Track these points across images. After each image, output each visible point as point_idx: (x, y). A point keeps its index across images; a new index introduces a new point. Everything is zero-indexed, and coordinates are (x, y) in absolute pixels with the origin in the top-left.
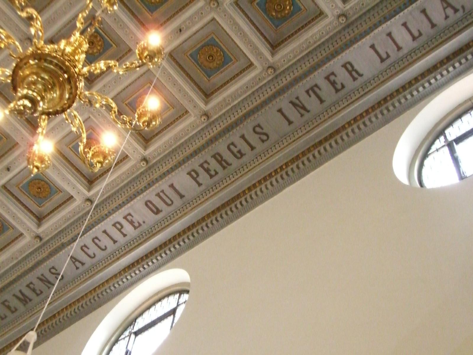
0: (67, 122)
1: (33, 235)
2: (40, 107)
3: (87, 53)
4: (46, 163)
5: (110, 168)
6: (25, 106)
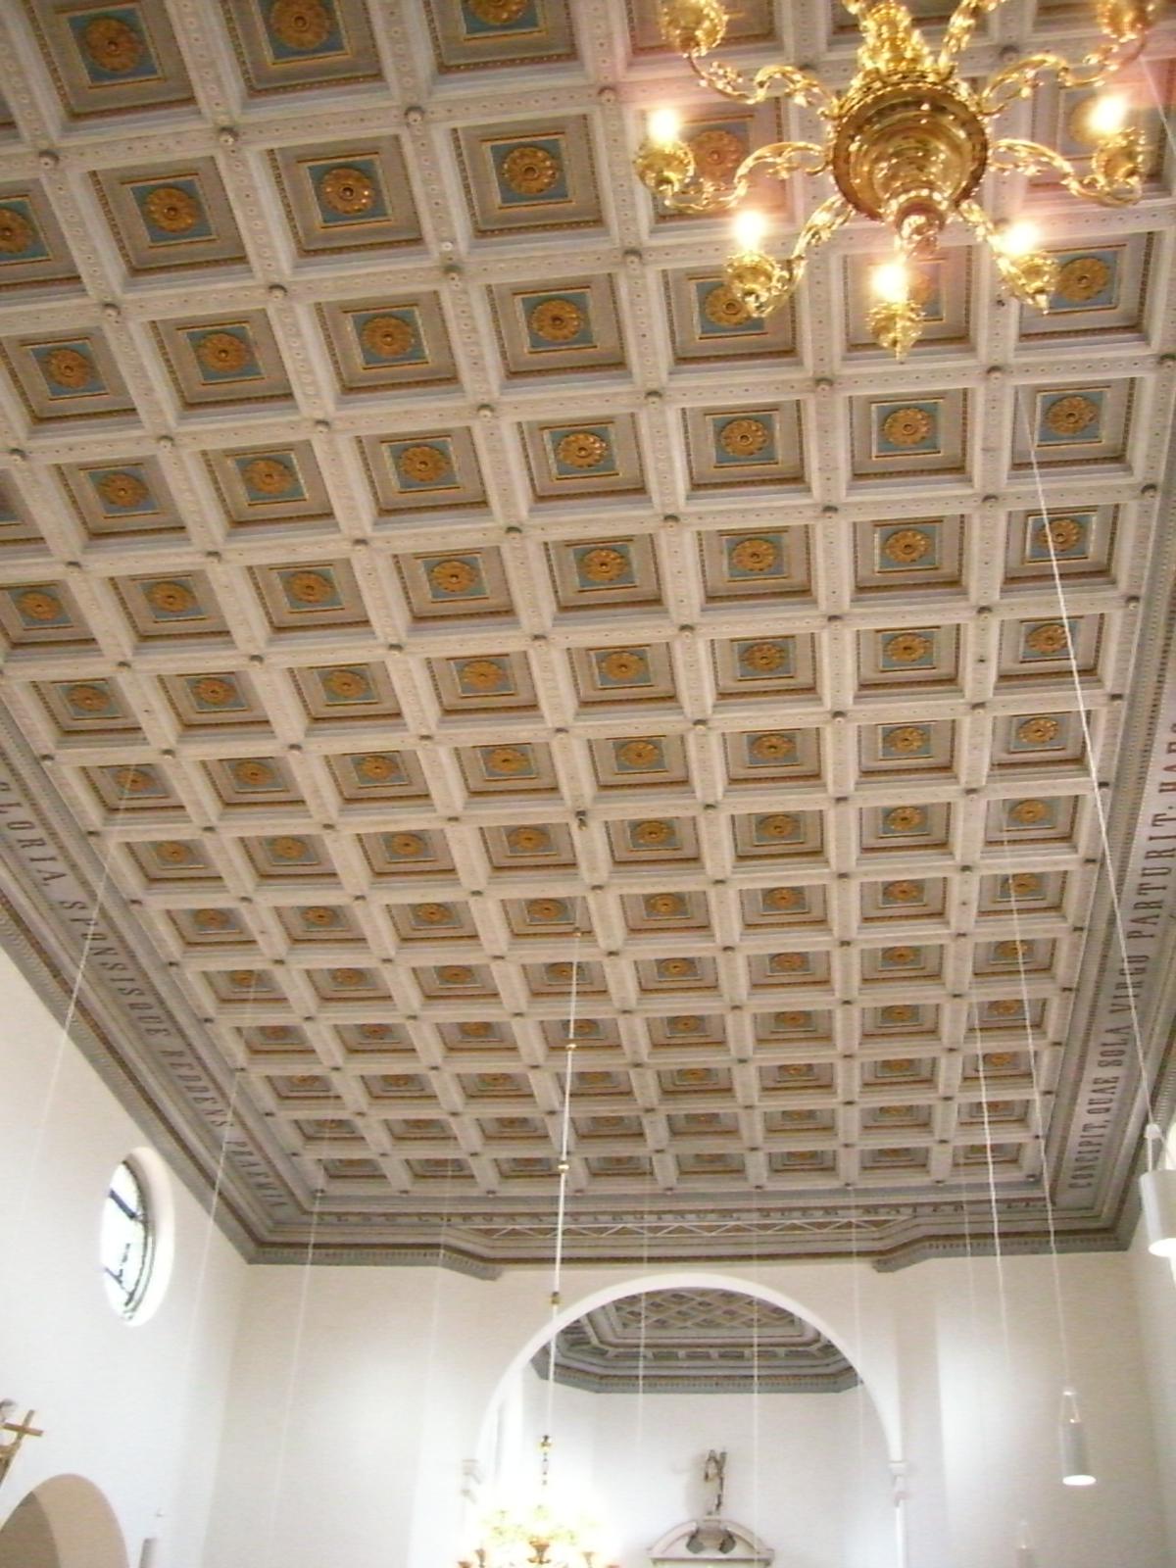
0: (1006, 174)
1: (1150, 363)
2: (940, 203)
3: (917, 22)
4: (1046, 269)
5: (1163, 131)
6: (918, 230)
